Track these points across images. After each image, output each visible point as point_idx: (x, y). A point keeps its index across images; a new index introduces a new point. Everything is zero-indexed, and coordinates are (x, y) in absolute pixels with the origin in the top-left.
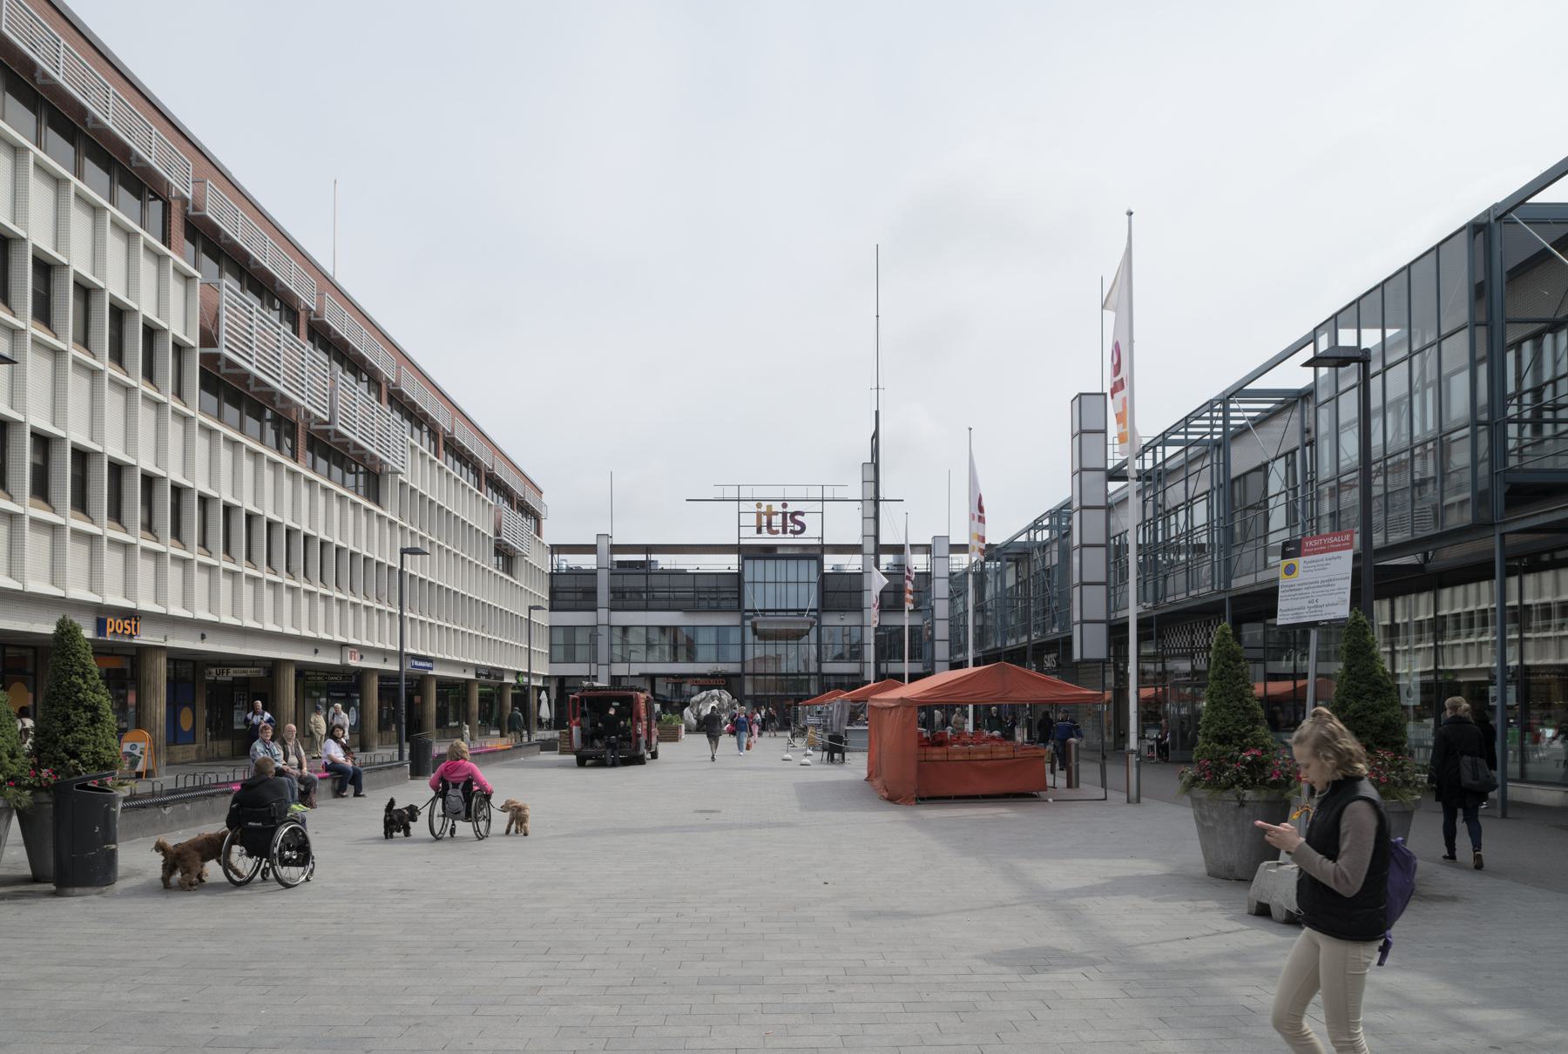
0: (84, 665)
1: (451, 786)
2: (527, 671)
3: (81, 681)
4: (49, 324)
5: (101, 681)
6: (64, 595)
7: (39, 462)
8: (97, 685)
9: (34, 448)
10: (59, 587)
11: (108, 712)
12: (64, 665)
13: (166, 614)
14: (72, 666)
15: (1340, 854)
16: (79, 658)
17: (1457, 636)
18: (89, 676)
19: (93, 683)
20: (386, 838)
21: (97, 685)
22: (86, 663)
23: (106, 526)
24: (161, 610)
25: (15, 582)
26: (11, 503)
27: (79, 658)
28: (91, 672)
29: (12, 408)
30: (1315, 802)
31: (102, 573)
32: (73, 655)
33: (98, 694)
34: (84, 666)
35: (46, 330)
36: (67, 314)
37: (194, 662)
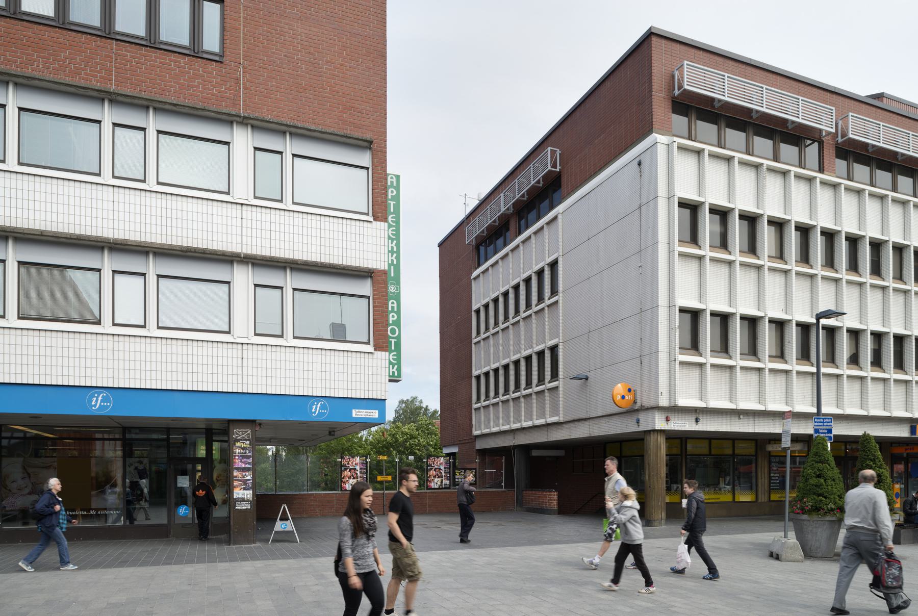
0: (874, 455)
1: (130, 493)
2: (815, 410)
3: (871, 463)
4: (529, 279)
5: (884, 463)
6: (890, 415)
7: (877, 348)
8: (881, 465)
9: (826, 338)
10: (841, 409)
11: (887, 477)
12: (865, 455)
13: (867, 416)
14: (868, 456)
15: (859, 487)
16: (871, 452)
17: (664, 44)
18: (877, 460)
19: (879, 464)
20: (462, 541)
21: (881, 465)
22: (875, 454)
23: (892, 373)
24: (887, 414)
25: (864, 411)
26: (884, 374)
27: (871, 452)
28: (878, 458)
29: (861, 324)
30: (660, 391)
31: (912, 401)
32: (869, 450)
33: (881, 469)
34: (874, 455)
35: (878, 278)
36: (889, 269)
37: (681, 438)
